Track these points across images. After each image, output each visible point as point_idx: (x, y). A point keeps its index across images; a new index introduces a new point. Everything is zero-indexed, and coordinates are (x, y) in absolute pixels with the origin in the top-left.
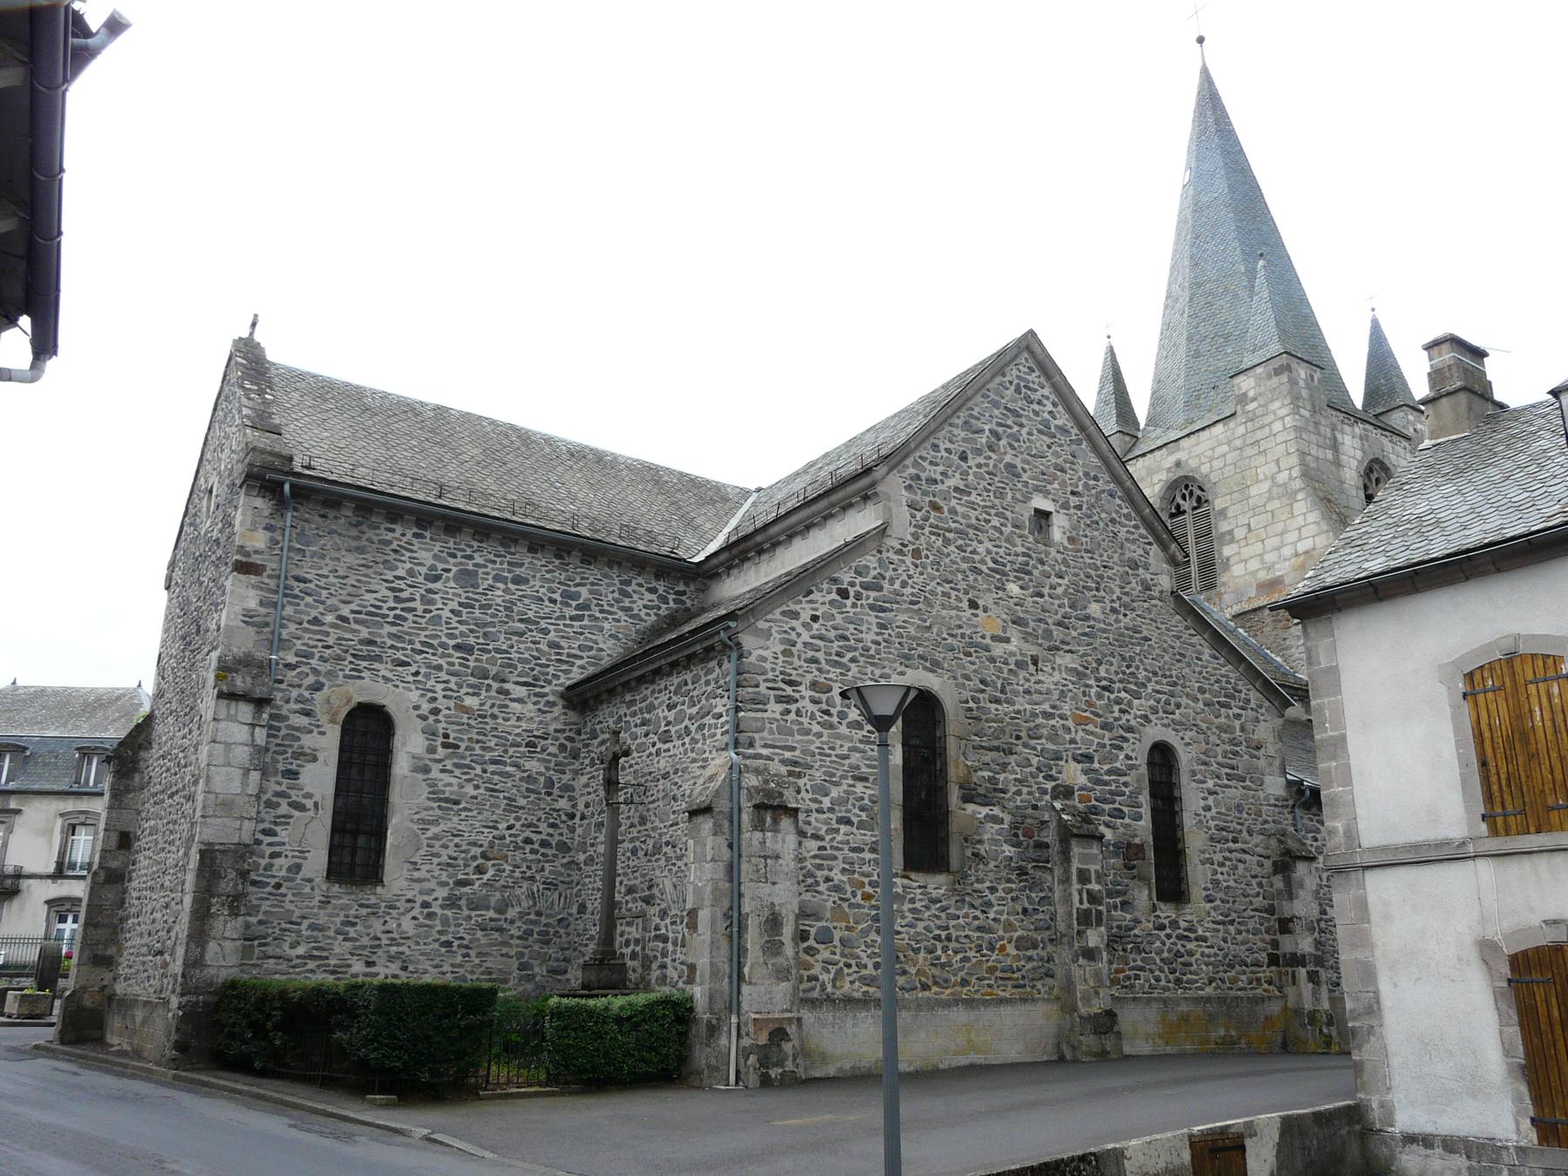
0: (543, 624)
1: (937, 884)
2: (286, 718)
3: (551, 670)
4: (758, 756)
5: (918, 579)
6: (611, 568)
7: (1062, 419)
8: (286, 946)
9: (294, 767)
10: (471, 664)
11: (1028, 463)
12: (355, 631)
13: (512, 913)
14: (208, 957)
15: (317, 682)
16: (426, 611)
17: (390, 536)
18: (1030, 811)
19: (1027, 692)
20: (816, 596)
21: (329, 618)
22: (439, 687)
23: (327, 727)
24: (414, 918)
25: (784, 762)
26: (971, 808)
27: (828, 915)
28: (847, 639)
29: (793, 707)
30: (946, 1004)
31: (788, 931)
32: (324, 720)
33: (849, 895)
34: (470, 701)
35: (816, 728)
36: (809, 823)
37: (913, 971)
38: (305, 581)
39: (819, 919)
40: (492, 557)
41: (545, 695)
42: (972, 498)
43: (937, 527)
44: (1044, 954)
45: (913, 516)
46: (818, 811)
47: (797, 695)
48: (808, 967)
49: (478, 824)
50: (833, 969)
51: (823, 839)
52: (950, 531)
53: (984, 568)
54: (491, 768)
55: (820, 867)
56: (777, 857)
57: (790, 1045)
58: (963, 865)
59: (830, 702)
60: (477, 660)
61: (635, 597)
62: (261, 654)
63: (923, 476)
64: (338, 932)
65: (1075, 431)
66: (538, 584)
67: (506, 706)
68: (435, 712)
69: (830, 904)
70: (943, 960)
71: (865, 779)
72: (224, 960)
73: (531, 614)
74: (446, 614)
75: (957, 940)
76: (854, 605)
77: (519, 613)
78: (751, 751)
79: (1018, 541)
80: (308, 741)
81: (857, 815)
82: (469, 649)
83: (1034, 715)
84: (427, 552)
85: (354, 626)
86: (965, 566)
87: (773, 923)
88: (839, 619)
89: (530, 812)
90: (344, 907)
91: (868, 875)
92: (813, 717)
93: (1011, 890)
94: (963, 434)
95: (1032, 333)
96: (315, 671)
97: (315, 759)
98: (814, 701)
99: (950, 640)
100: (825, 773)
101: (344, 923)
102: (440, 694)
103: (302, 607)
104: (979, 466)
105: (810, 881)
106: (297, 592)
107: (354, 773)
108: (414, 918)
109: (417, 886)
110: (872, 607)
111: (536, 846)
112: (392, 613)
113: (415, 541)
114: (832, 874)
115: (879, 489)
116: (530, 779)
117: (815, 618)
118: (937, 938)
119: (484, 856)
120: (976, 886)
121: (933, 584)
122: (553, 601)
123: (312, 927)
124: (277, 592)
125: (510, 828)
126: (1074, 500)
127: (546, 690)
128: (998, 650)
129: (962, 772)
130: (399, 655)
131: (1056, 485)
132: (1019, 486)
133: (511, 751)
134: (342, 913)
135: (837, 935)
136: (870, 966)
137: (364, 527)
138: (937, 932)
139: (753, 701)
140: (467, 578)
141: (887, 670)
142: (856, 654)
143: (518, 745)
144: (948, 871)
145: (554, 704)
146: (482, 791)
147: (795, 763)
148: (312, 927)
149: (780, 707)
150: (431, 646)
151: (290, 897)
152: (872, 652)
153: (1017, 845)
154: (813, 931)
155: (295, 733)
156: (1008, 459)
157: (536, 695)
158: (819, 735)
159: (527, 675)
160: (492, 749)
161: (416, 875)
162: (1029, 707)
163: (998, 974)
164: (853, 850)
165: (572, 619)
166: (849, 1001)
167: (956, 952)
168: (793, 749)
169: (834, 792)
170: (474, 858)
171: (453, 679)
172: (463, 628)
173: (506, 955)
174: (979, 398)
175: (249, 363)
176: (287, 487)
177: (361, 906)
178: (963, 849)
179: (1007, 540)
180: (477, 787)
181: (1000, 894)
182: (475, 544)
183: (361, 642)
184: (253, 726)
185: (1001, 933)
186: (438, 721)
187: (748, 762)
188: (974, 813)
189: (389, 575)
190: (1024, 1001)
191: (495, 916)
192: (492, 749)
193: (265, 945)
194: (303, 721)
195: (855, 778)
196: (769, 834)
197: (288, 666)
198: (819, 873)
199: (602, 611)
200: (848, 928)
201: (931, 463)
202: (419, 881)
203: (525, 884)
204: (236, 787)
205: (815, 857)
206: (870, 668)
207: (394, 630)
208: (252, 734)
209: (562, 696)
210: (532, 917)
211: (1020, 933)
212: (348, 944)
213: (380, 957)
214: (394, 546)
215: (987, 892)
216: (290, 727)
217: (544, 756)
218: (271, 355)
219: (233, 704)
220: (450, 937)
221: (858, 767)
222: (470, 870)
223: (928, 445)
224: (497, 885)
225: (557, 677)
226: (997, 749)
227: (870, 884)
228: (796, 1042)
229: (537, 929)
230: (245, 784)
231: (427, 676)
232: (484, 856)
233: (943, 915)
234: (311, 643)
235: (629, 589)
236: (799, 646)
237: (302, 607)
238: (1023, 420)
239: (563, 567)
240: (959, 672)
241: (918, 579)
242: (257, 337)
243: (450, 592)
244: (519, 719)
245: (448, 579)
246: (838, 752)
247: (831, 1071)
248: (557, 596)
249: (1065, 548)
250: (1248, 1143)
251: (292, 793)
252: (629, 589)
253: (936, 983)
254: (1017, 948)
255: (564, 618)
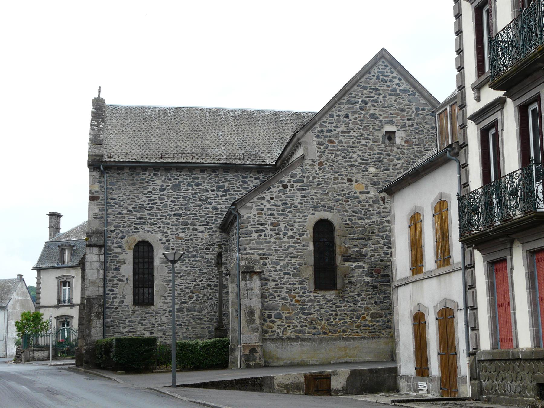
0: (209, 200)
1: (330, 295)
2: (113, 250)
3: (214, 218)
4: (249, 253)
5: (321, 174)
6: (237, 172)
7: (404, 85)
8: (121, 329)
9: (117, 267)
10: (181, 221)
11: (382, 111)
12: (134, 215)
13: (204, 312)
14: (92, 333)
15: (123, 235)
16: (161, 203)
17: (144, 177)
18: (379, 262)
19: (379, 213)
20: (272, 189)
21: (125, 212)
22: (169, 231)
23: (128, 251)
24: (166, 316)
25: (259, 254)
26: (347, 264)
27: (280, 308)
28: (287, 204)
29: (263, 234)
30: (335, 340)
31: (257, 315)
32: (126, 249)
33: (289, 301)
34: (182, 235)
35: (273, 240)
36: (271, 276)
37: (319, 327)
38: (114, 199)
39: (277, 310)
40: (186, 177)
41: (213, 228)
42: (351, 134)
43: (331, 150)
44: (386, 319)
45: (319, 148)
46: (274, 271)
47: (264, 229)
48: (272, 327)
49: (188, 281)
50: (282, 328)
51: (277, 281)
52: (338, 151)
53: (356, 164)
54: (192, 259)
55: (276, 292)
56: (252, 290)
57: (258, 354)
58: (343, 286)
59: (280, 230)
60: (183, 219)
61: (249, 183)
62: (101, 228)
63: (325, 130)
64: (139, 323)
65: (411, 89)
66: (206, 184)
67: (197, 235)
68: (168, 240)
69: (280, 305)
70: (334, 323)
71: (297, 257)
72: (96, 332)
73: (204, 197)
74: (169, 203)
75: (340, 315)
76: (290, 190)
77: (199, 197)
78: (245, 252)
79: (376, 148)
80: (121, 257)
81: (292, 271)
82: (180, 215)
83: (382, 222)
84: (159, 181)
85: (134, 213)
86: (346, 164)
87: (251, 312)
88: (283, 197)
89: (209, 274)
90: (140, 314)
91: (297, 293)
92: (272, 236)
93: (369, 295)
94: (346, 106)
95: (384, 50)
96: (122, 232)
97: (125, 263)
98: (272, 230)
99: (338, 197)
100: (277, 257)
101: (140, 320)
102: (169, 234)
103: (114, 209)
104: (356, 118)
105: (271, 297)
106: (112, 204)
107: (141, 266)
108: (166, 316)
109: (167, 305)
110: (298, 190)
111: (212, 287)
112: (148, 206)
113: (154, 177)
114: (281, 294)
115: (302, 140)
116: (208, 262)
117: (272, 198)
118: (331, 315)
119: (192, 292)
120: (350, 294)
121: (330, 175)
122: (213, 191)
123: (130, 322)
124: (104, 205)
125: (201, 281)
126: (408, 123)
127: (212, 226)
128: (363, 197)
129: (343, 250)
130: (152, 221)
131: (399, 118)
132: (377, 123)
133: (200, 252)
134: (140, 316)
135: (284, 316)
136: (299, 326)
137: (134, 175)
138: (331, 313)
139: (245, 233)
140: (176, 187)
141: (306, 214)
142: (291, 209)
143: (202, 249)
144: (337, 290)
145: (216, 232)
146: (189, 268)
147: (264, 254)
148: (130, 322)
149: (257, 234)
150: (164, 216)
151: (121, 312)
152: (299, 207)
153: (372, 276)
154: (273, 315)
155: (117, 255)
156: (371, 112)
157: (208, 229)
158: (275, 243)
159: (204, 222)
160: (192, 252)
161: (166, 301)
162: (379, 219)
163: (362, 328)
164: (291, 284)
165: (221, 196)
166: (289, 339)
167: (340, 320)
168: (263, 249)
169: (282, 264)
170: (188, 293)
171: (174, 227)
172: (176, 207)
173: (203, 328)
174: (355, 87)
175: (99, 109)
176: (102, 167)
177: (146, 313)
178: (343, 280)
179: (369, 149)
180: (187, 267)
181: (363, 296)
182: (178, 173)
183: (137, 219)
184: (99, 255)
185: (363, 312)
186: (169, 244)
187: (243, 256)
188: (349, 266)
189: (146, 192)
190: (374, 338)
191: (198, 314)
192: (192, 252)
193: (114, 328)
194: (119, 250)
195: (291, 257)
196: (248, 282)
197: (112, 231)
198: (275, 294)
199: (234, 191)
200: (289, 313)
201: (329, 123)
202: (167, 303)
203: (209, 302)
204: (95, 276)
205: (273, 288)
206: (298, 214)
207: (149, 212)
208: (99, 258)
209: (219, 228)
210: (213, 313)
211: (373, 311)
212: (143, 327)
213: (155, 331)
214: (146, 180)
215: (356, 296)
216: (114, 253)
217: (213, 252)
218: (108, 102)
219: (91, 248)
220: (180, 323)
221: (292, 253)
222: (187, 298)
223: (327, 116)
224: (198, 302)
225: (217, 221)
226: (362, 239)
227: (299, 296)
228: (260, 353)
229: (215, 318)
230: (98, 275)
231: (164, 227)
232: (192, 292)
233: (334, 306)
234: (119, 222)
235: (246, 180)
236: (265, 210)
237: (114, 209)
238: (381, 92)
239: (216, 176)
240: (342, 210)
241: (321, 174)
242: (101, 96)
243: (169, 192)
244: (202, 239)
245: (169, 189)
246: (283, 248)
247: (282, 363)
248: (215, 188)
249: (403, 146)
250: (333, 378)
251: (118, 276)
252: (246, 180)
253: (330, 332)
254: (371, 317)
255: (218, 196)
